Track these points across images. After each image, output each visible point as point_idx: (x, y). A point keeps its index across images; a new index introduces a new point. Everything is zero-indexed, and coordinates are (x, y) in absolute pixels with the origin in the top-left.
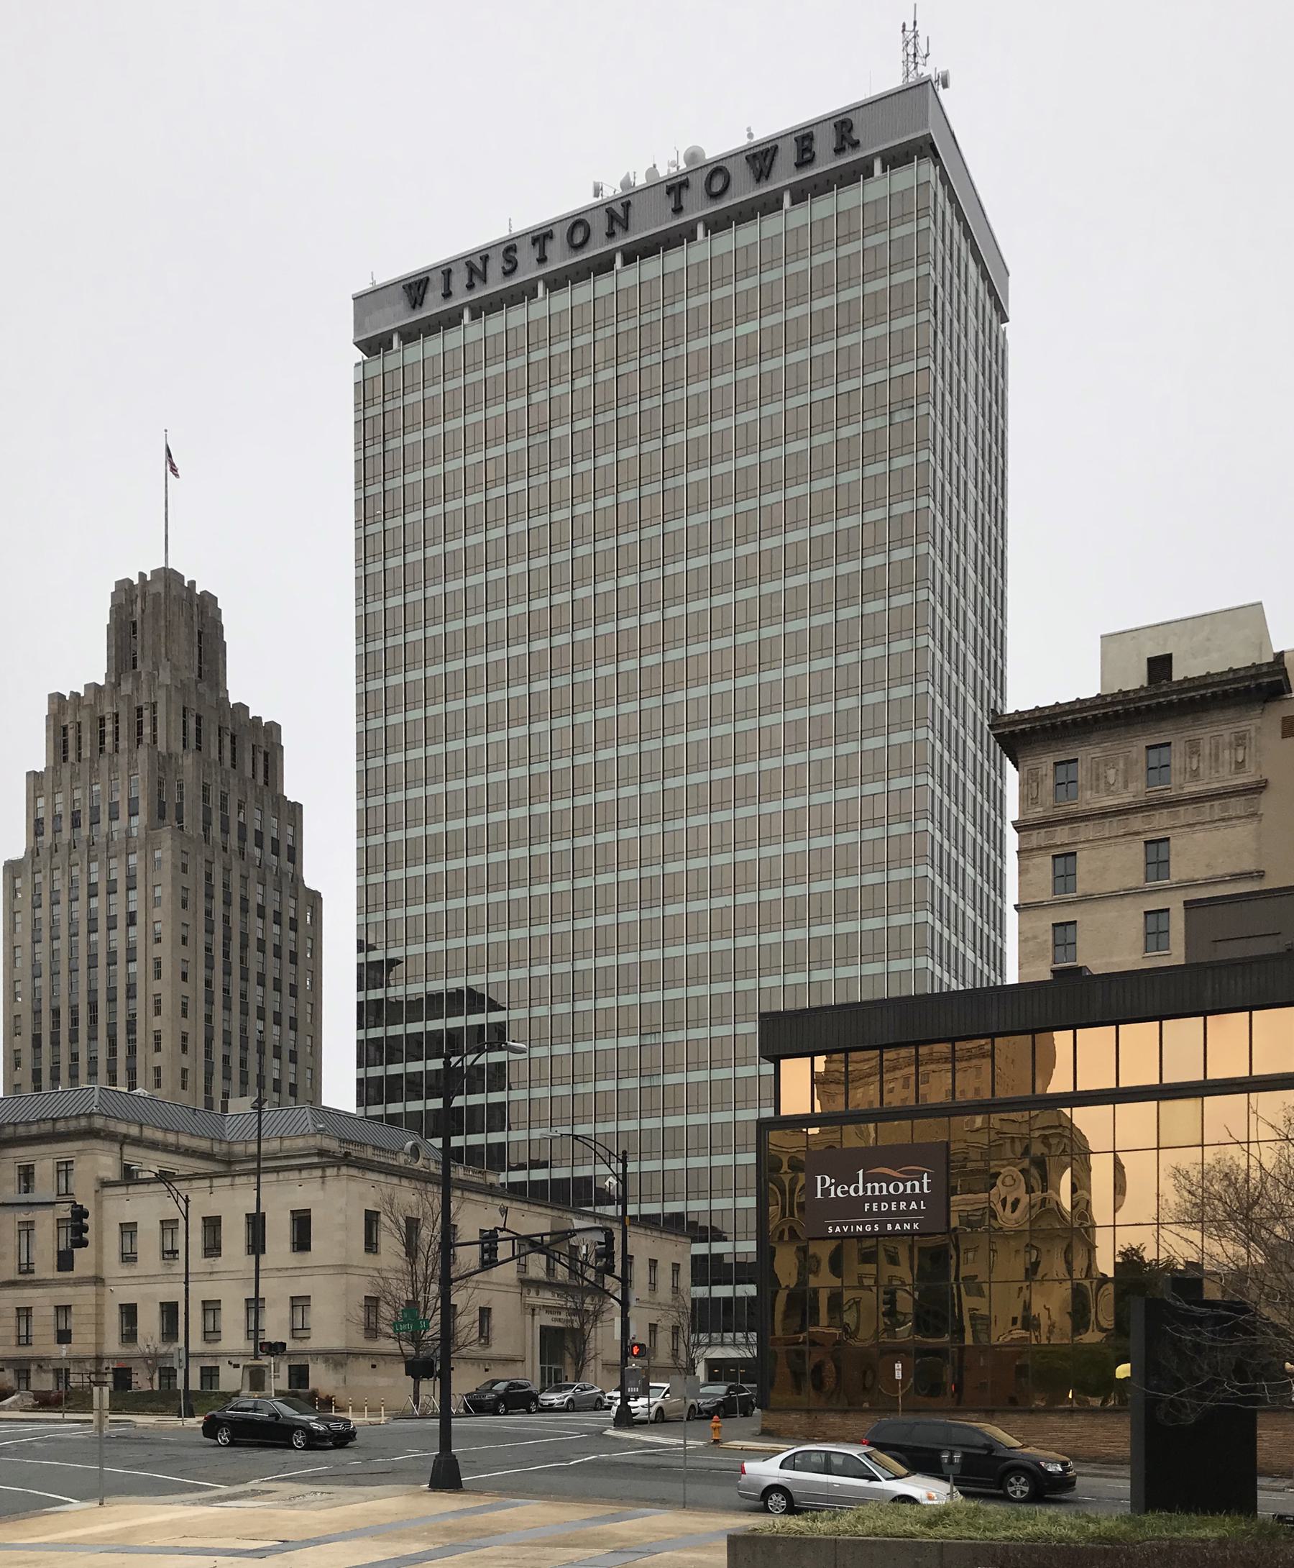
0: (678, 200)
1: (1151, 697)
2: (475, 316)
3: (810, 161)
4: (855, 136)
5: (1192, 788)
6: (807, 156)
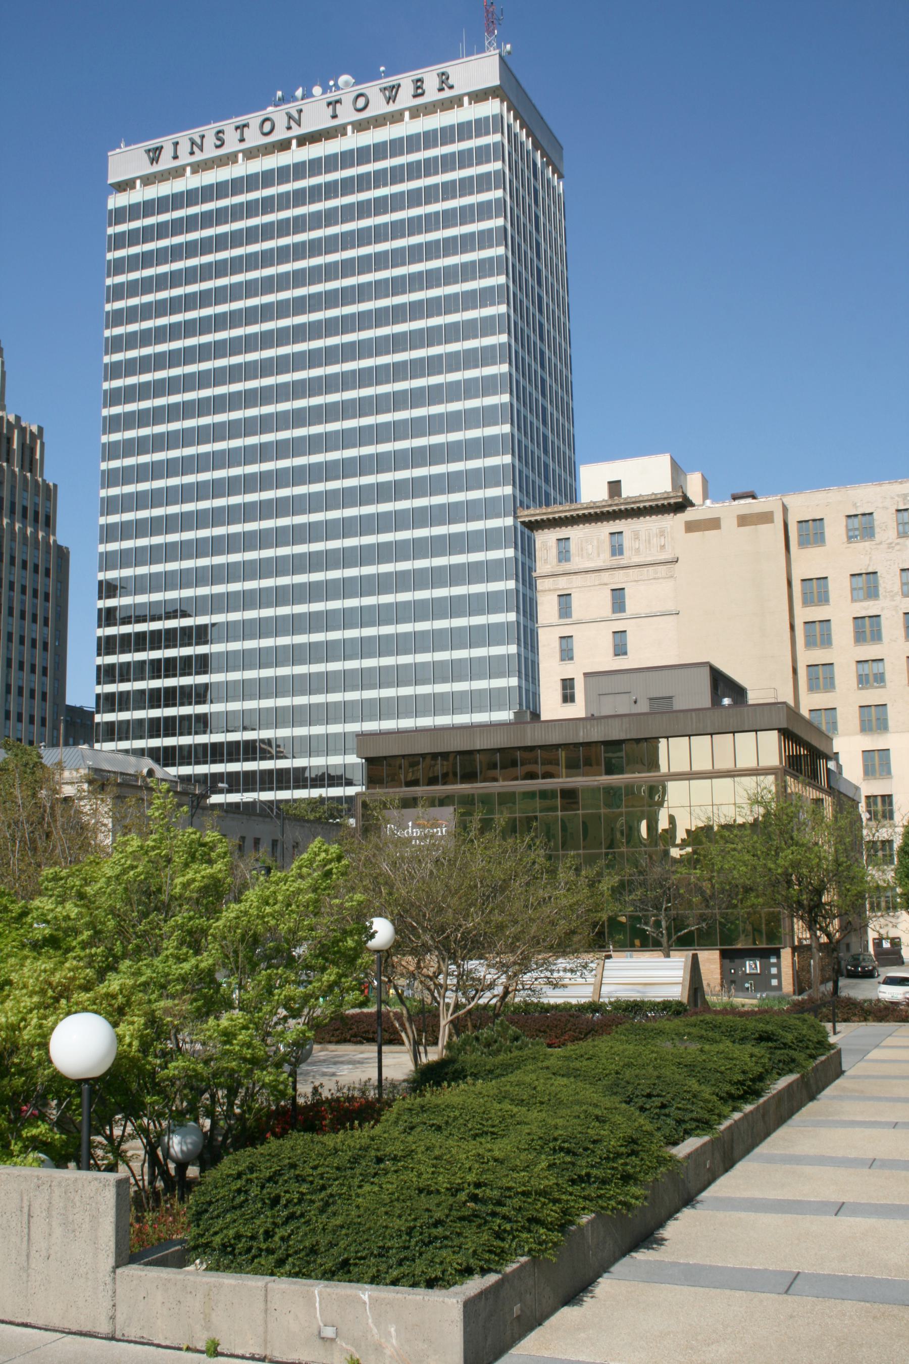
0: (334, 110)
1: (610, 505)
2: (194, 172)
3: (422, 94)
4: (451, 82)
5: (636, 560)
6: (420, 91)
